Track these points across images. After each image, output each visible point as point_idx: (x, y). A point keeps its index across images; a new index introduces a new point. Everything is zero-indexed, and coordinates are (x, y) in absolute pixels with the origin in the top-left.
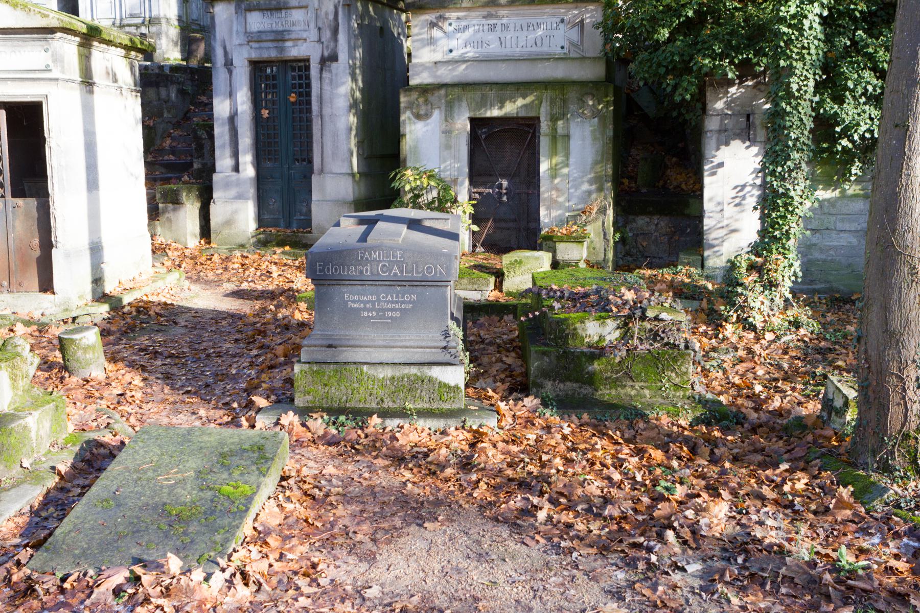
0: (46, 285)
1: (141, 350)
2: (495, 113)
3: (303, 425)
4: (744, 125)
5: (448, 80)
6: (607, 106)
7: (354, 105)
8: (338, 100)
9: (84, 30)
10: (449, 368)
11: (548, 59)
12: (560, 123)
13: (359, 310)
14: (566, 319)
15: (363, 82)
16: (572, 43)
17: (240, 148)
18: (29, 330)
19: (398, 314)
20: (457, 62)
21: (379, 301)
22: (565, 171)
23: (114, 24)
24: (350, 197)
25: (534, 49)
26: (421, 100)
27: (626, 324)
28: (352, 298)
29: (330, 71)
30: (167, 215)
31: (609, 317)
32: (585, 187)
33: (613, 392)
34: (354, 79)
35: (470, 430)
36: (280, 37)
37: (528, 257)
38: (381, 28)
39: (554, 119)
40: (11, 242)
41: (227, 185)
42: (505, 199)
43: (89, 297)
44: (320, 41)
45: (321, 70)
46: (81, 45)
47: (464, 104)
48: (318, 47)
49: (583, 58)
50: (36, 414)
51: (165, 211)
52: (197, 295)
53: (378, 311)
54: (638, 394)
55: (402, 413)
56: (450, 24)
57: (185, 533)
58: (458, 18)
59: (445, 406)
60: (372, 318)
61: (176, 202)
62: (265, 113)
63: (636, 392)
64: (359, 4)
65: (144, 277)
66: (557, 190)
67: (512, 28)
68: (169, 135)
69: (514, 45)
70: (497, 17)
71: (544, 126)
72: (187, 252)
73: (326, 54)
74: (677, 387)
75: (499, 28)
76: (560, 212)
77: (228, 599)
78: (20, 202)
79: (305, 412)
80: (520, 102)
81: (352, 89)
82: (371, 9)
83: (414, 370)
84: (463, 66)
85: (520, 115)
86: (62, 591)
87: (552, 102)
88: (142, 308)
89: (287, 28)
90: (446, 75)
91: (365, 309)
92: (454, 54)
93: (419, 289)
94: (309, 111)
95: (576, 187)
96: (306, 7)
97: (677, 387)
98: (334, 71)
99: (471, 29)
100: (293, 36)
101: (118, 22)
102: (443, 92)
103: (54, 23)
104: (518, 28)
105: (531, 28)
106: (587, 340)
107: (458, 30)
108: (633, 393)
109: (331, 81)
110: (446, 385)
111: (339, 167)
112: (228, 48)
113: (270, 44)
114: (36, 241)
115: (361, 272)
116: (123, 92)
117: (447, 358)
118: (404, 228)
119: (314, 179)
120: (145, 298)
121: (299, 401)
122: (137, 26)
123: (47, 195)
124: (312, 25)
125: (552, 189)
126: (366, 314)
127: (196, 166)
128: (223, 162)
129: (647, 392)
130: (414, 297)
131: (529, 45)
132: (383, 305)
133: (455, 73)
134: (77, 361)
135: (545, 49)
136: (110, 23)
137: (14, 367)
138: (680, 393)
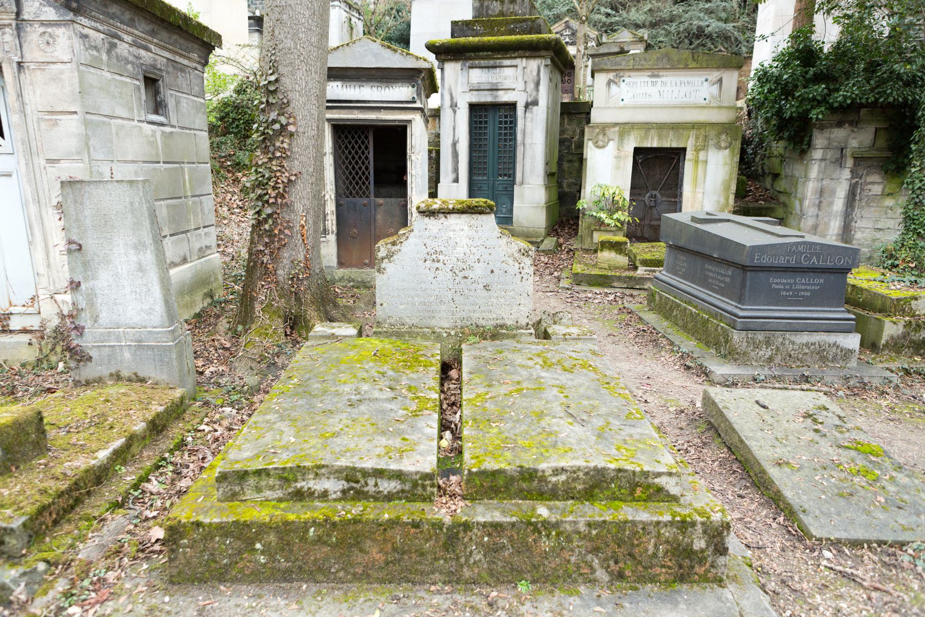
4: (839, 156)
13: (780, 290)
21: (795, 283)
25: (684, 99)
29: (532, 112)
39: (697, 150)
49: (720, 107)
60: (789, 296)
70: (658, 76)
71: (689, 155)
73: (529, 100)
75: (659, 84)
87: (697, 138)
93: (827, 275)
94: (515, 139)
104: (674, 84)
109: (532, 119)
115: (788, 261)
124: (520, 79)
126: (785, 293)
130: (822, 281)
132: (798, 287)
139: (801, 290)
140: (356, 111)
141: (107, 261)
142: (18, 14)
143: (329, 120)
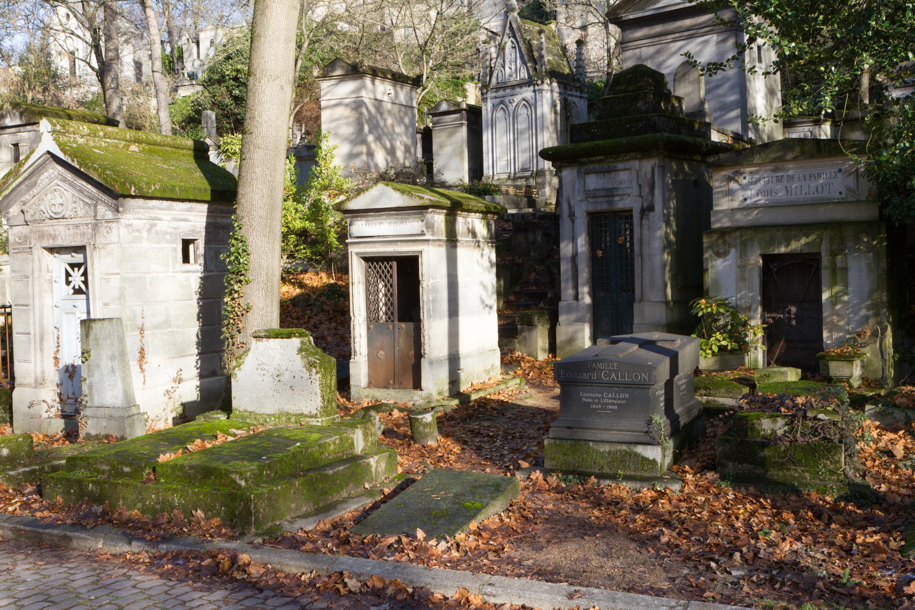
0: (417, 385)
1: (469, 431)
2: (783, 250)
3: (545, 480)
5: (742, 224)
6: (880, 243)
7: (668, 245)
8: (655, 241)
9: (448, 203)
10: (649, 447)
11: (828, 204)
12: (839, 257)
13: (590, 403)
14: (746, 417)
15: (677, 226)
16: (848, 189)
17: (580, 282)
18: (402, 415)
19: (616, 407)
20: (750, 208)
21: (603, 397)
22: (846, 298)
23: (509, 177)
24: (664, 321)
25: (816, 195)
26: (720, 242)
27: (792, 422)
28: (585, 395)
29: (648, 219)
30: (524, 334)
31: (778, 416)
32: (864, 312)
33: (781, 473)
34: (668, 224)
35: (656, 491)
36: (610, 193)
37: (775, 372)
38: (696, 181)
39: (833, 254)
40: (396, 353)
41: (570, 310)
42: (794, 323)
43: (447, 394)
44: (640, 195)
45: (642, 218)
46: (447, 215)
47: (756, 243)
48: (639, 200)
49: (859, 202)
50: (376, 457)
51: (522, 331)
52: (531, 397)
53: (603, 404)
54: (800, 476)
55: (613, 477)
56: (745, 178)
57: (435, 524)
58: (751, 173)
59: (646, 475)
60: (598, 409)
61: (530, 325)
62: (600, 253)
63: (796, 473)
64: (673, 164)
65: (492, 381)
66: (838, 315)
67: (796, 179)
68: (535, 270)
69: (799, 193)
70: (784, 170)
71: (825, 261)
72: (537, 364)
73: (645, 205)
74: (832, 472)
75: (785, 179)
76: (841, 334)
77: (445, 556)
78: (403, 325)
79: (547, 473)
80: (804, 241)
81: (666, 233)
82: (686, 166)
83: (624, 447)
84: (756, 212)
85: (803, 251)
86: (363, 543)
87: (831, 241)
88: (483, 403)
89: (615, 186)
90: (742, 219)
91: (593, 403)
92: (748, 202)
95: (856, 313)
96: (630, 169)
97: (832, 472)
98: (651, 219)
99: (762, 182)
100: (620, 192)
101: (512, 175)
102: (738, 233)
103: (427, 203)
105: (813, 178)
106: (762, 433)
107: (752, 183)
108: (796, 475)
109: (649, 226)
110: (647, 459)
111: (654, 296)
112: (572, 203)
113: (603, 199)
114: (412, 353)
116: (481, 245)
117: (648, 439)
118: (636, 347)
119: (636, 306)
120: (488, 397)
121: (547, 465)
122: (527, 178)
123: (420, 320)
124: (634, 183)
125: (833, 315)
127: (549, 295)
128: (567, 292)
129: (807, 475)
130: (627, 396)
131: (811, 192)
132: (606, 401)
133: (750, 218)
134: (420, 433)
135: (826, 195)
136: (506, 176)
137: (365, 428)
138: (835, 477)
139: (609, 404)
140: (377, 245)
141: (98, 366)
142: (95, 216)
143: (357, 254)
